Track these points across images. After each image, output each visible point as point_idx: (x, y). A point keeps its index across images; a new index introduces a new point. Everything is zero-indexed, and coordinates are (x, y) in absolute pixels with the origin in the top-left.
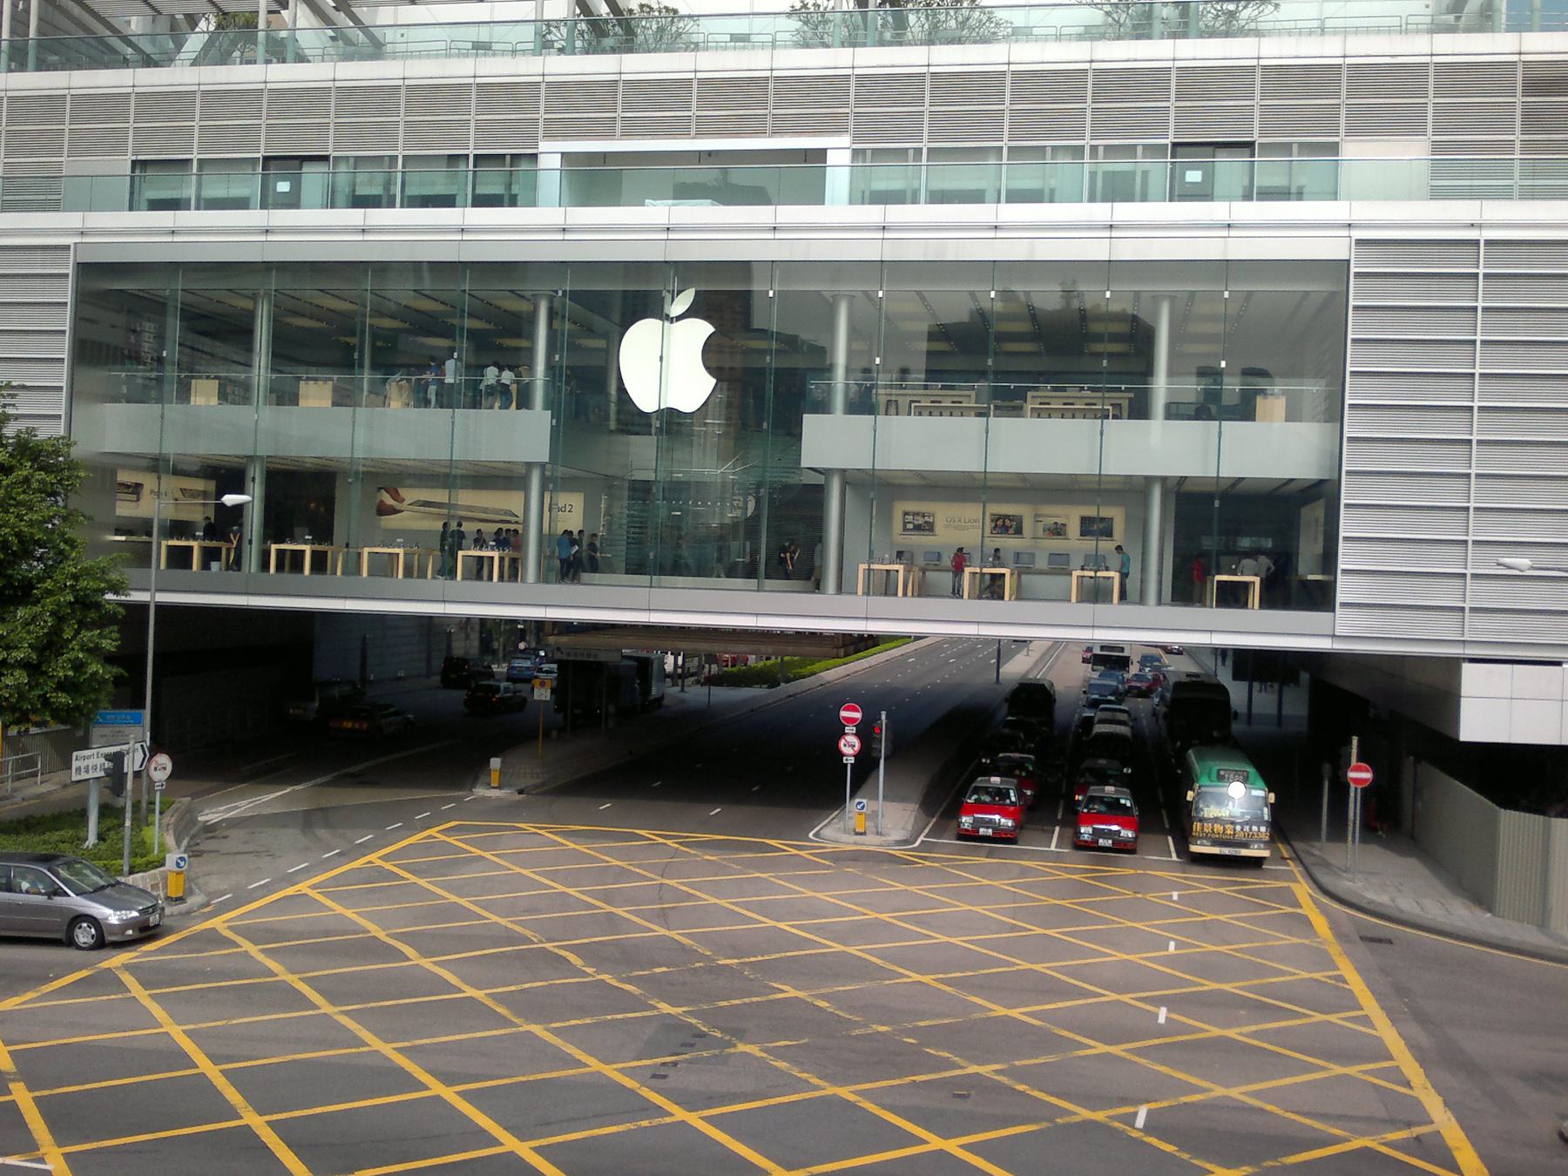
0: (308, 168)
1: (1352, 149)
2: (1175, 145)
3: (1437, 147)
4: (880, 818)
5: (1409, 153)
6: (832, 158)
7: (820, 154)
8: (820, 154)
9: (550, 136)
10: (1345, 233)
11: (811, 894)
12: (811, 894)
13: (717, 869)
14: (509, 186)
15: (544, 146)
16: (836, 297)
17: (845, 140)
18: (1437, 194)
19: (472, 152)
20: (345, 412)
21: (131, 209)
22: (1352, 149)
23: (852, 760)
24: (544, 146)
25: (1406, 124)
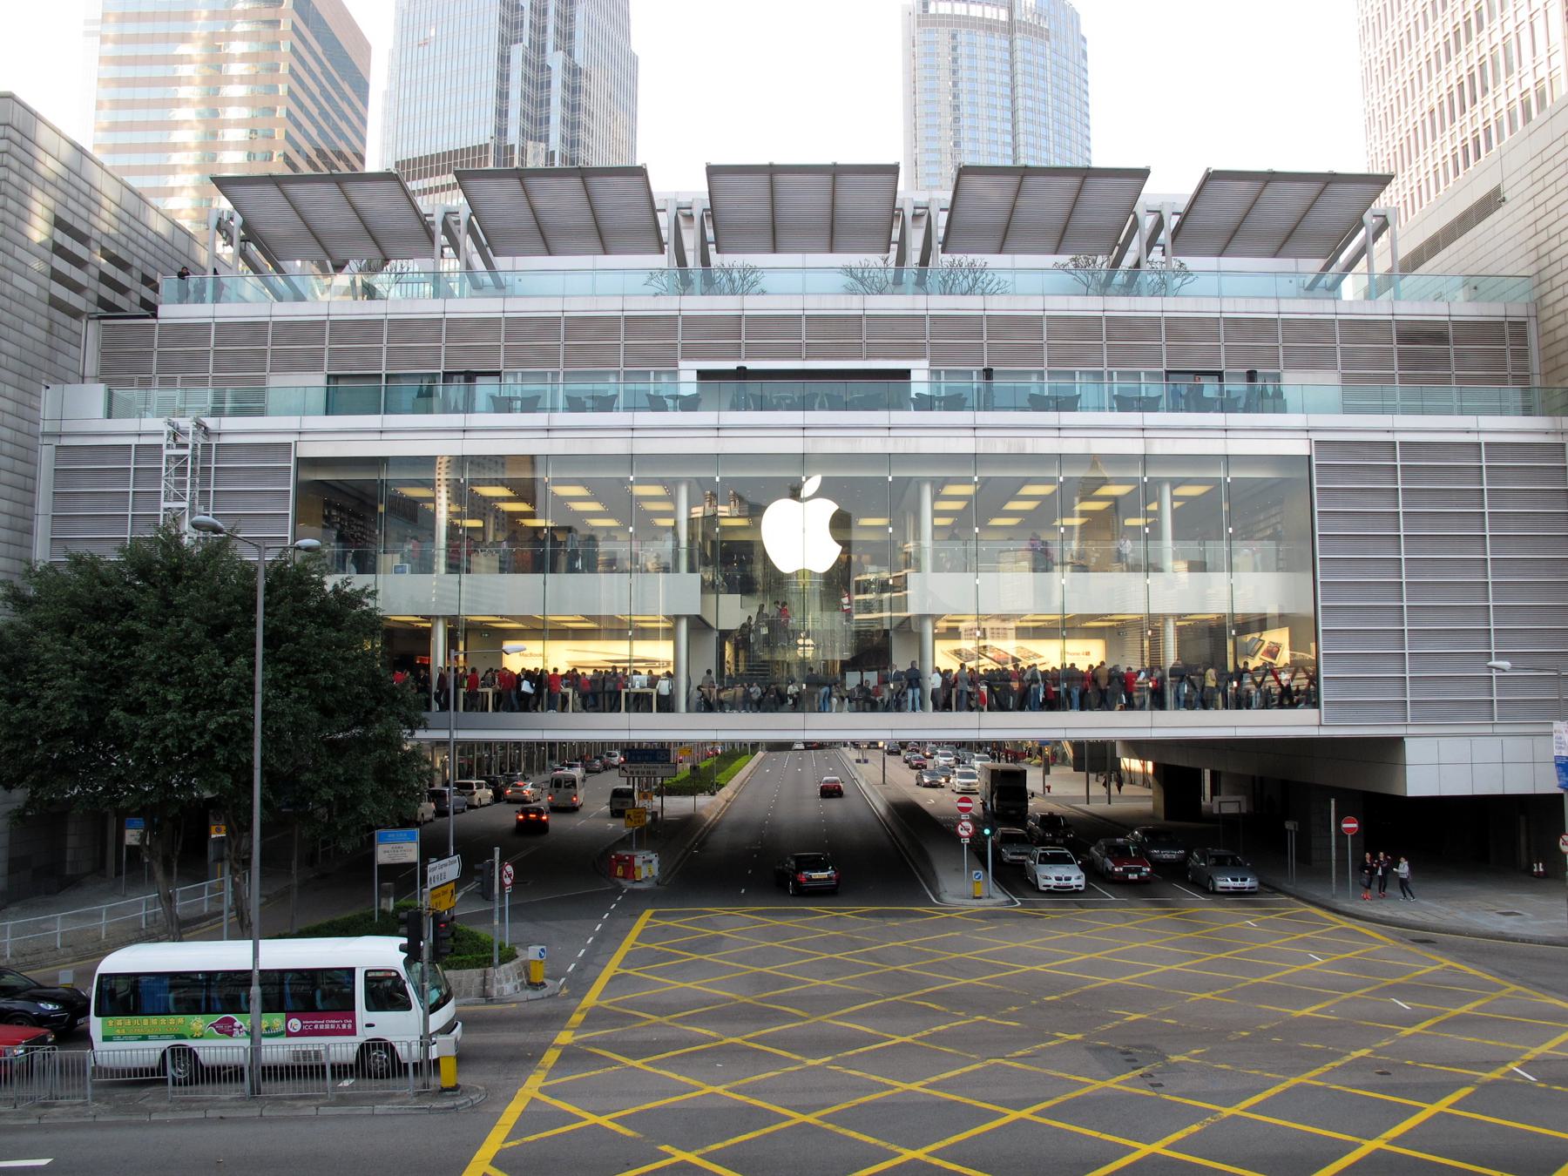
0: (479, 380)
1: (275, 381)
2: (1168, 372)
3: (1345, 378)
4: (965, 888)
5: (1326, 382)
6: (914, 376)
7: (905, 374)
8: (905, 374)
9: (685, 357)
10: (1304, 435)
11: (681, 985)
12: (681, 985)
13: (981, 925)
14: (989, 389)
15: (682, 364)
16: (919, 482)
17: (925, 364)
18: (1347, 410)
19: (384, 372)
20: (455, 577)
21: (327, 413)
22: (275, 381)
23: (967, 841)
24: (682, 364)
25: (310, 363)
